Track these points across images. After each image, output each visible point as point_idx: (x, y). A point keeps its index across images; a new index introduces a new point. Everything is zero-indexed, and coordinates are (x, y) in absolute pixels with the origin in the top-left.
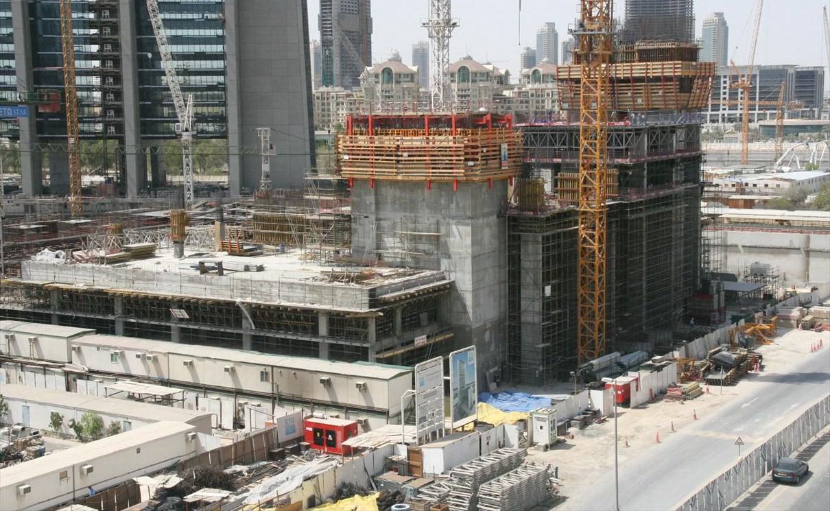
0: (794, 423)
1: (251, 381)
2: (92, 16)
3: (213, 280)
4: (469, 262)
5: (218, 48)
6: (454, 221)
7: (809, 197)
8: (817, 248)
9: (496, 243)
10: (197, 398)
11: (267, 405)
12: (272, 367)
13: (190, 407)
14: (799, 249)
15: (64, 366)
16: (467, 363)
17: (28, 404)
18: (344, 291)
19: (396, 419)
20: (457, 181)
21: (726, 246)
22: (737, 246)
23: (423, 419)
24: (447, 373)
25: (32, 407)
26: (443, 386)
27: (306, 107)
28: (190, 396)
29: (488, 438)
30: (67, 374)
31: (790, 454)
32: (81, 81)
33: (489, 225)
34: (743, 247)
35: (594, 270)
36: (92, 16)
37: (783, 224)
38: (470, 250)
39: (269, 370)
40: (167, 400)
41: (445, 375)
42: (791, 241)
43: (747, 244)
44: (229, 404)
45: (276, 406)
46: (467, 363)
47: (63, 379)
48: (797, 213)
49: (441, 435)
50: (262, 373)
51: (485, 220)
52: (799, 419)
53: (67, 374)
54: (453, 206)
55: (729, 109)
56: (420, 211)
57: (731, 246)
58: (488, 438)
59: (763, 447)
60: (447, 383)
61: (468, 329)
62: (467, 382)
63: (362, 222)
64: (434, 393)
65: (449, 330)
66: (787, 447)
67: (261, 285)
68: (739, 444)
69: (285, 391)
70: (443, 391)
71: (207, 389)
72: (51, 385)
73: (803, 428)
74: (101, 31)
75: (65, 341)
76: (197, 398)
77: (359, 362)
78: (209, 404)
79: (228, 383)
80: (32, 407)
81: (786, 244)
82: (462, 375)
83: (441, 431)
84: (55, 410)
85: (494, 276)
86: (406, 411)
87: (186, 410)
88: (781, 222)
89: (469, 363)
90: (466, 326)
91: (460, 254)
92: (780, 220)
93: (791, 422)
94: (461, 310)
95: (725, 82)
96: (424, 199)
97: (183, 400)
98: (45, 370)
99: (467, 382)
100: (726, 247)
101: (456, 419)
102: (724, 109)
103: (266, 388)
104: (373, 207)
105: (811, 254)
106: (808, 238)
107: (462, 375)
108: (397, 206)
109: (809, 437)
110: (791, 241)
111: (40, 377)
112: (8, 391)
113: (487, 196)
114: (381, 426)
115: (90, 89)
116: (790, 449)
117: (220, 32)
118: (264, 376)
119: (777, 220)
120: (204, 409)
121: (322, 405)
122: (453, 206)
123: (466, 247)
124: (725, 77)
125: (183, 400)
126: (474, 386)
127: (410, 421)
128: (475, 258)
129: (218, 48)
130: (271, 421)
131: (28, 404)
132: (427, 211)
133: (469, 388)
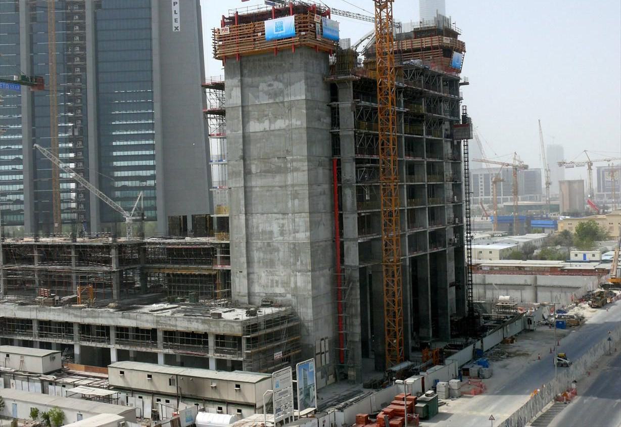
0: (527, 403)
1: (163, 386)
2: (71, 145)
3: (138, 317)
4: (310, 301)
5: (151, 163)
6: (300, 274)
7: (535, 251)
8: (542, 284)
9: (329, 288)
10: (127, 397)
11: (173, 402)
12: (177, 375)
13: (123, 404)
14: (531, 285)
15: (40, 376)
16: (309, 371)
17: (16, 402)
18: (225, 323)
19: (261, 410)
20: (294, 46)
21: (485, 284)
22: (491, 284)
23: (279, 410)
24: (294, 378)
25: (19, 404)
26: (292, 387)
27: (208, 199)
28: (123, 396)
29: (324, 421)
30: (42, 381)
31: (525, 424)
32: (64, 186)
33: (323, 276)
34: (496, 284)
35: (394, 305)
36: (71, 145)
37: (520, 270)
38: (311, 293)
39: (175, 377)
40: (107, 399)
41: (296, 383)
42: (526, 281)
43: (498, 283)
44: (148, 401)
45: (180, 402)
46: (309, 371)
47: (39, 385)
48: (528, 261)
49: (292, 420)
50: (170, 380)
51: (321, 272)
52: (530, 400)
53: (42, 381)
54: (299, 263)
55: (485, 195)
56: (277, 267)
57: (488, 284)
58: (324, 421)
59: (507, 421)
60: (295, 385)
61: (311, 346)
62: (309, 383)
63: (238, 275)
64: (287, 392)
65: (298, 347)
66: (523, 419)
67: (170, 320)
68: (492, 419)
69: (185, 392)
70: (292, 390)
71: (133, 391)
72: (32, 389)
73: (533, 406)
74: (76, 154)
75: (41, 359)
76: (127, 397)
77: (236, 371)
78: (135, 401)
79: (147, 386)
80: (19, 404)
81: (522, 282)
82: (305, 379)
83: (292, 417)
84: (34, 406)
85: (327, 311)
86: (267, 405)
87: (120, 407)
88: (520, 268)
89: (310, 371)
90: (309, 345)
91: (304, 295)
92: (518, 267)
93: (525, 403)
94: (306, 334)
95: (481, 178)
96: (279, 259)
97: (118, 399)
98: (28, 379)
99: (309, 383)
100: (485, 285)
101: (301, 410)
102: (482, 196)
103: (172, 390)
104: (245, 265)
105: (538, 288)
106: (536, 278)
107: (305, 379)
108: (261, 264)
109: (537, 412)
110: (526, 281)
111: (25, 384)
112: (5, 393)
113: (321, 256)
114: (251, 415)
115: (69, 191)
116: (525, 421)
117: (152, 152)
118: (171, 382)
119: (516, 267)
120: (132, 405)
121: (211, 401)
122: (299, 263)
123: (309, 290)
124: (481, 175)
125: (118, 399)
126: (314, 386)
127: (270, 411)
128: (314, 298)
129: (151, 163)
130: (176, 413)
131: (16, 402)
132: (281, 267)
133: (310, 387)
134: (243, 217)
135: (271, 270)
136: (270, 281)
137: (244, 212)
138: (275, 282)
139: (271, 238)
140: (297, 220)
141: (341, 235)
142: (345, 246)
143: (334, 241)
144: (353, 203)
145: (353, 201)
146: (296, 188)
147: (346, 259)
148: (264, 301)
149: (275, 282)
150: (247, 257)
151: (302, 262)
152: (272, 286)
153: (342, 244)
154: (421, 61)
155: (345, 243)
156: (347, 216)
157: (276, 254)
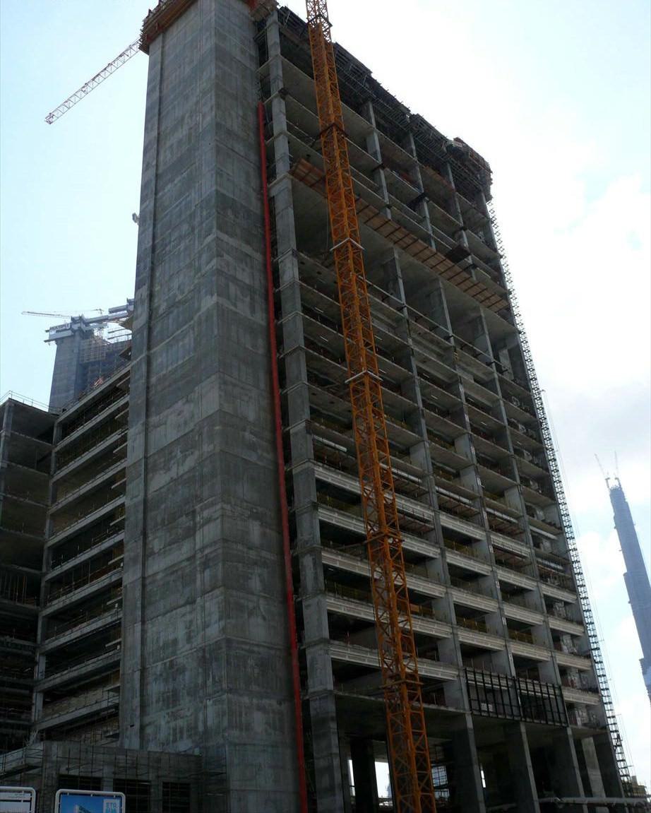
134: (138, 627)
135: (174, 710)
136: (171, 731)
137: (140, 619)
138: (178, 731)
139: (174, 653)
140: (207, 605)
141: (300, 639)
142: (309, 657)
143: (288, 650)
144: (316, 578)
145: (316, 573)
146: (207, 551)
147: (310, 682)
148: (110, 716)
149: (178, 731)
150: (142, 696)
151: (213, 678)
152: (175, 741)
153: (302, 656)
154: (433, 514)
155: (307, 652)
156: (307, 603)
157: (181, 677)
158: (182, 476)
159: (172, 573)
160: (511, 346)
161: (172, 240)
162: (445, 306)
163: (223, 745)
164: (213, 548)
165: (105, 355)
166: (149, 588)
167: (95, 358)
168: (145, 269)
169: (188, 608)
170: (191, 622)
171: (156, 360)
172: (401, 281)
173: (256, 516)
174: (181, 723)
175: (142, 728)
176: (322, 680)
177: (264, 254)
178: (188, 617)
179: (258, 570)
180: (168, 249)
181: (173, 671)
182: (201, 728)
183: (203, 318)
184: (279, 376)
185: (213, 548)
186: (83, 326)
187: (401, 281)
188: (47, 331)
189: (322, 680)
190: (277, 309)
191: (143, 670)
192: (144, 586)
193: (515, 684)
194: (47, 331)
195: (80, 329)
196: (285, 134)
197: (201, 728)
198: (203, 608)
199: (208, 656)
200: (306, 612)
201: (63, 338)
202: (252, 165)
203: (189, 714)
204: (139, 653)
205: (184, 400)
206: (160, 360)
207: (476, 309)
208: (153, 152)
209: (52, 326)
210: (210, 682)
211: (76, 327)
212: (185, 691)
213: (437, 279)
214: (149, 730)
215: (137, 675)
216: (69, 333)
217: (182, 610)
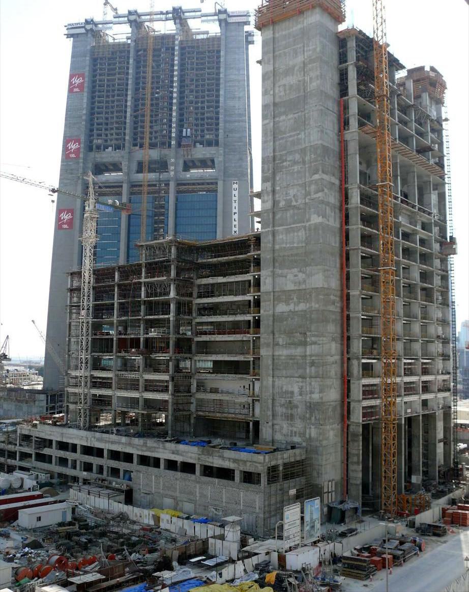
140: (313, 383)
141: (348, 396)
142: (352, 406)
147: (351, 417)
150: (273, 411)
151: (315, 417)
158: (297, 312)
159: (291, 359)
160: (441, 191)
161: (288, 159)
162: (416, 184)
163: (319, 447)
164: (317, 358)
165: (110, 53)
166: (276, 361)
167: (103, 54)
168: (269, 170)
169: (300, 380)
170: (302, 387)
171: (279, 236)
172: (399, 178)
173: (333, 339)
174: (295, 429)
175: (273, 425)
176: (357, 417)
177: (341, 181)
178: (301, 384)
179: (334, 366)
180: (285, 164)
181: (290, 405)
182: (307, 436)
183: (313, 227)
184: (346, 258)
185: (317, 358)
186: (94, 28)
187: (399, 178)
188: (66, 26)
189: (357, 417)
190: (346, 219)
191: (273, 399)
192: (273, 359)
193: (225, 100)
194: (66, 26)
195: (92, 30)
196: (356, 97)
197: (307, 436)
198: (310, 384)
199: (312, 406)
200: (352, 386)
201: (78, 34)
202: (335, 115)
203: (300, 427)
204: (271, 391)
205: (299, 269)
206: (281, 237)
207: (429, 176)
208: (270, 82)
209: (69, 23)
210: (313, 418)
211: (89, 27)
212: (298, 416)
213: (414, 166)
214: (277, 427)
215: (270, 401)
216: (83, 31)
217: (297, 379)
